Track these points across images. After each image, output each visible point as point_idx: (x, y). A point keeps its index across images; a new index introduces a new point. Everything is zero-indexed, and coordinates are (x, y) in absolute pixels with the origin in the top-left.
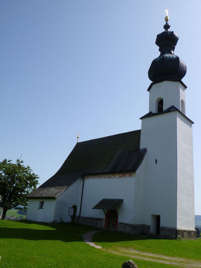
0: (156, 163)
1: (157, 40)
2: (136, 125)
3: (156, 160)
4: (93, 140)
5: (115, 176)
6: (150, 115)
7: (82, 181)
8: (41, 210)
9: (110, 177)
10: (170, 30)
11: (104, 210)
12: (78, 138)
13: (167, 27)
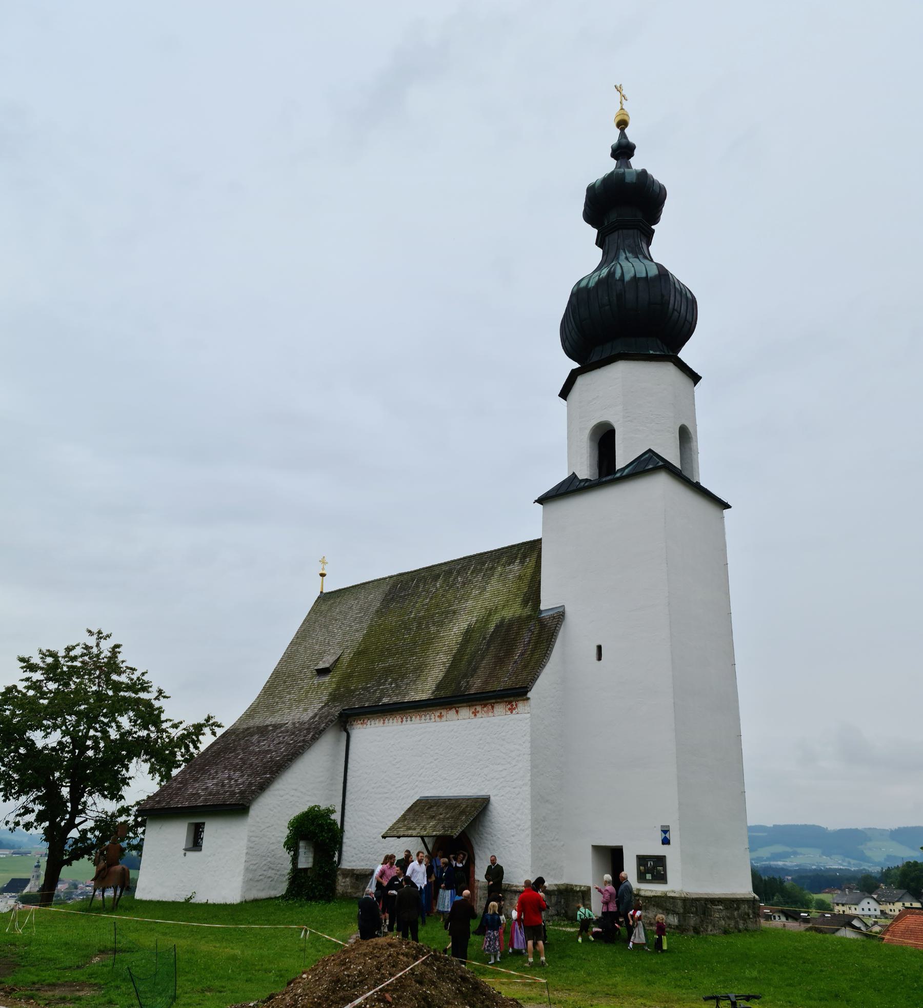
0: (599, 658)
1: (586, 204)
2: (527, 525)
3: (599, 648)
4: (801, 826)
5: (457, 712)
6: (569, 489)
7: (345, 734)
8: (191, 855)
9: (440, 716)
10: (637, 163)
11: (422, 837)
12: (323, 575)
13: (623, 151)
